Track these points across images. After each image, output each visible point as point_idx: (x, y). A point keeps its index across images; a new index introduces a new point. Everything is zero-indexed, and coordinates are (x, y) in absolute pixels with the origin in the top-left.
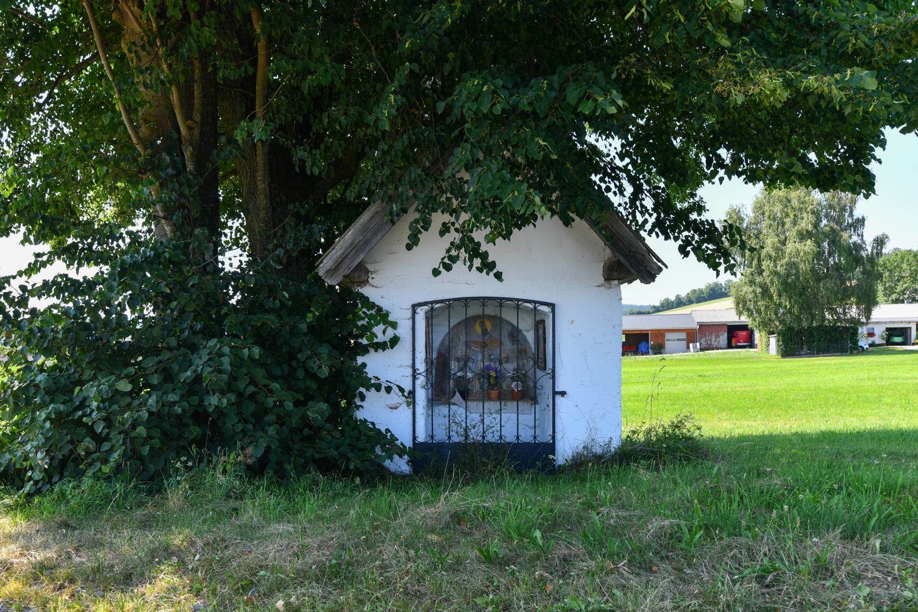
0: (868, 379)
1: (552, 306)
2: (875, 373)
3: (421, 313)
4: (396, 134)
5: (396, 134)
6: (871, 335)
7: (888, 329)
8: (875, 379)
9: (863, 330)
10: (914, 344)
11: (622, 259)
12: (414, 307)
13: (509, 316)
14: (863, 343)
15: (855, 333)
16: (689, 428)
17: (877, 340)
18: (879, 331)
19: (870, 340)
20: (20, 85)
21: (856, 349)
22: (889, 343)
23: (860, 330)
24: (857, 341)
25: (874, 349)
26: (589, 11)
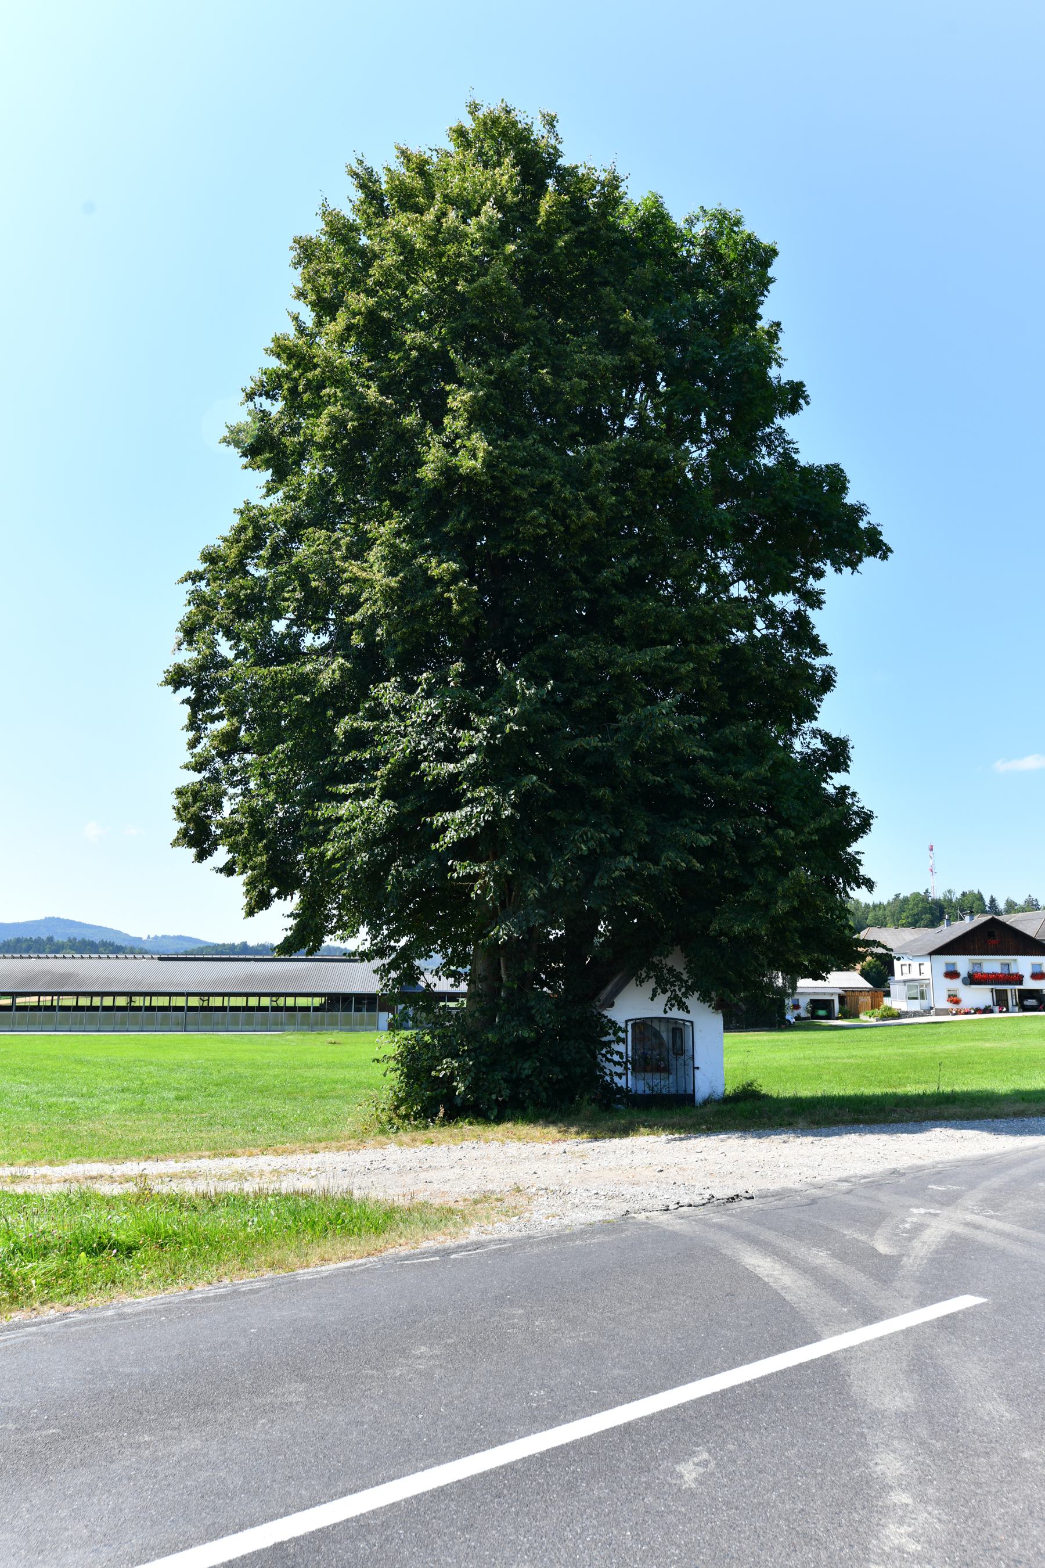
0: (805, 1059)
1: (692, 1023)
2: (808, 1053)
3: (630, 1024)
4: (250, 777)
5: (250, 777)
6: (796, 1007)
7: (812, 1001)
8: (810, 1059)
9: (789, 1002)
10: (837, 1019)
11: (231, 840)
12: (627, 1021)
13: (656, 1025)
14: (790, 1017)
15: (782, 1006)
16: (756, 1087)
17: (804, 1014)
18: (804, 1002)
19: (796, 1012)
20: (378, 639)
21: (784, 1024)
22: (815, 1016)
23: (786, 1001)
24: (785, 1014)
25: (802, 1024)
26: (880, 1389)
